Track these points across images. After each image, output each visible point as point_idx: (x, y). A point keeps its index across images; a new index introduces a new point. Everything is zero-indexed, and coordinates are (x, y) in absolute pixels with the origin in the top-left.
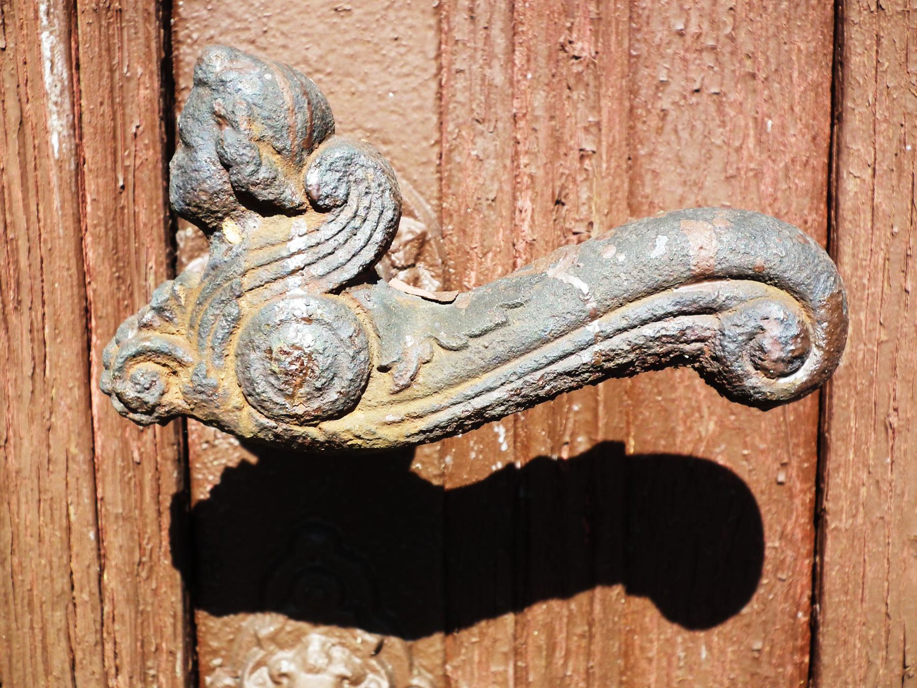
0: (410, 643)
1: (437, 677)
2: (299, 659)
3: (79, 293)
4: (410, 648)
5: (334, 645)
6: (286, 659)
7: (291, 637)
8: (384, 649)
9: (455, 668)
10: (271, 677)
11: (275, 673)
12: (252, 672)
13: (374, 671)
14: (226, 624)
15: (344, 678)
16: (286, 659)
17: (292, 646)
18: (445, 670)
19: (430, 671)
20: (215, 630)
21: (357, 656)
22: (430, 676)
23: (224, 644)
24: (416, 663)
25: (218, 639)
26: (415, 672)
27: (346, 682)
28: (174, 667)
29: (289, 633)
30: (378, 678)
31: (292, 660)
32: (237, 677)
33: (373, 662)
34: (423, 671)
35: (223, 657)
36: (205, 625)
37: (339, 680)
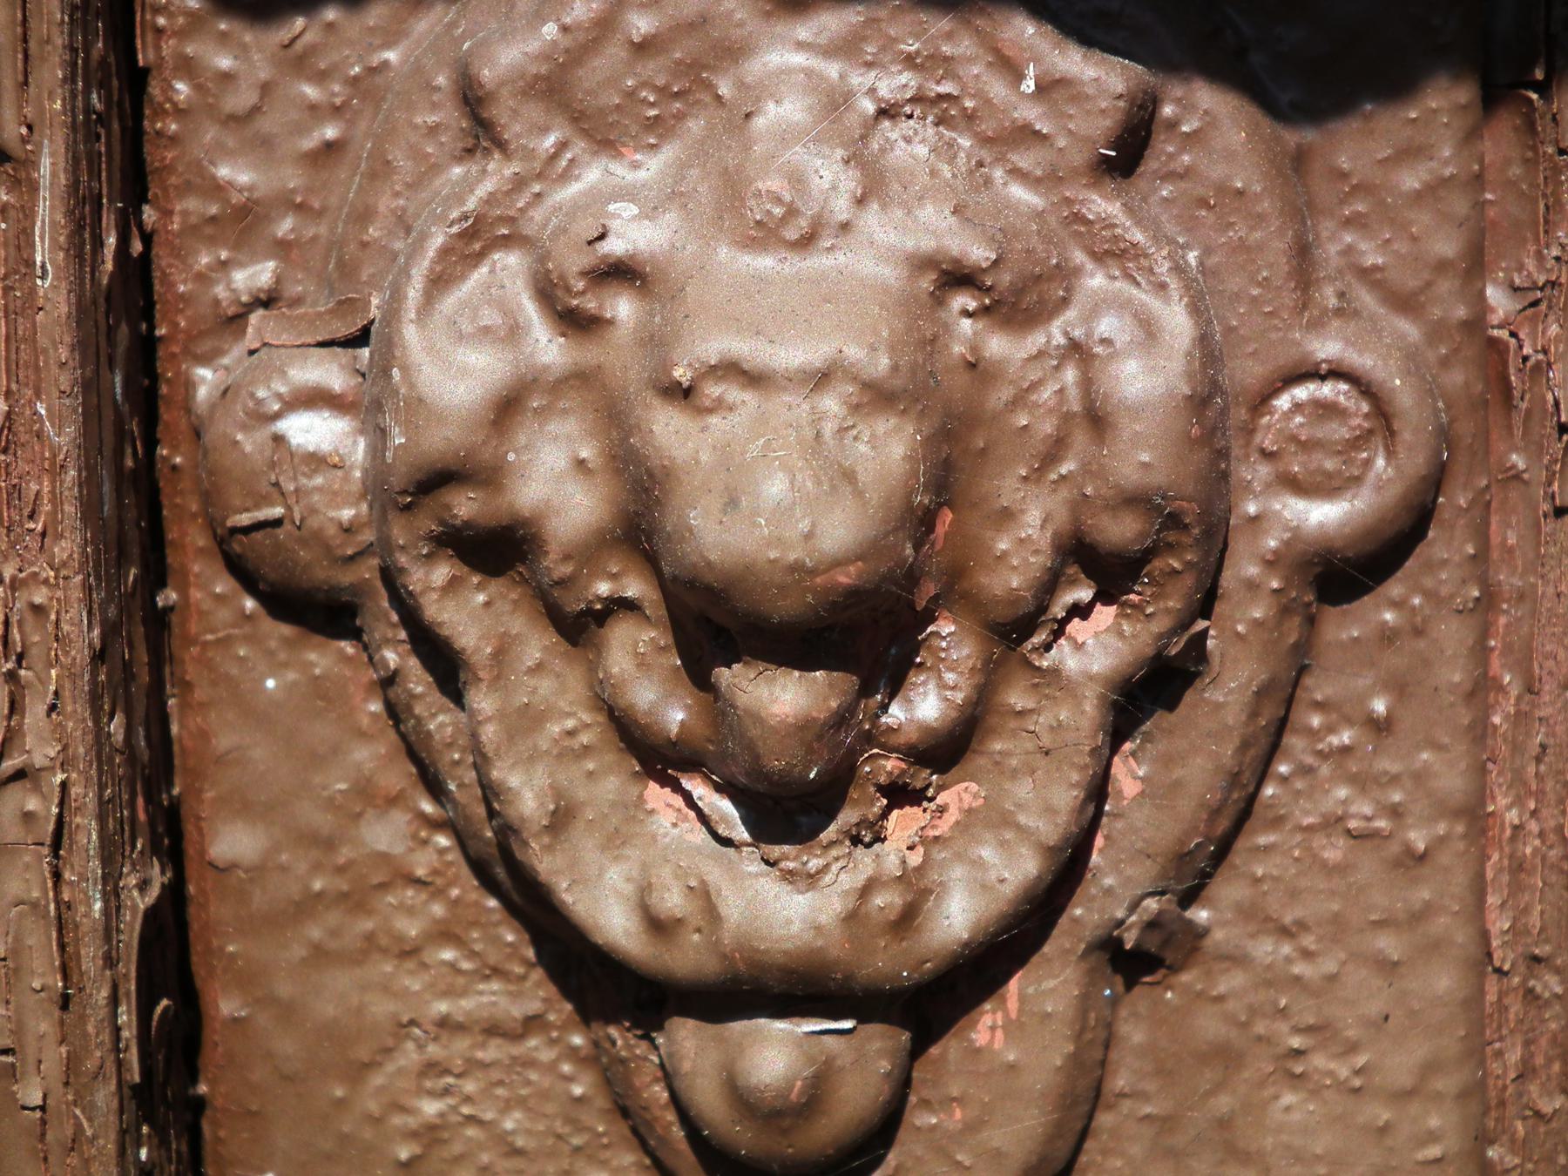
0: (1292, 137)
1: (1436, 333)
2: (704, 190)
3: (100, 736)
4: (1300, 160)
5: (887, 112)
6: (627, 194)
7: (655, 70)
8: (1163, 148)
9: (1534, 300)
10: (547, 291)
11: (572, 262)
12: (439, 282)
13: (1115, 254)
14: (299, 62)
15: (957, 277)
16: (627, 194)
17: (660, 128)
18: (1481, 307)
19: (1405, 303)
20: (241, 99)
21: (1016, 173)
22: (1410, 330)
23: (293, 179)
24: (1333, 244)
25: (263, 148)
26: (1328, 296)
27: (963, 300)
28: (23, 240)
29: (643, 48)
30: (1144, 297)
31: (673, 195)
32: (361, 338)
33: (1102, 205)
34: (1367, 299)
35: (283, 249)
36: (187, 67)
37: (926, 283)
